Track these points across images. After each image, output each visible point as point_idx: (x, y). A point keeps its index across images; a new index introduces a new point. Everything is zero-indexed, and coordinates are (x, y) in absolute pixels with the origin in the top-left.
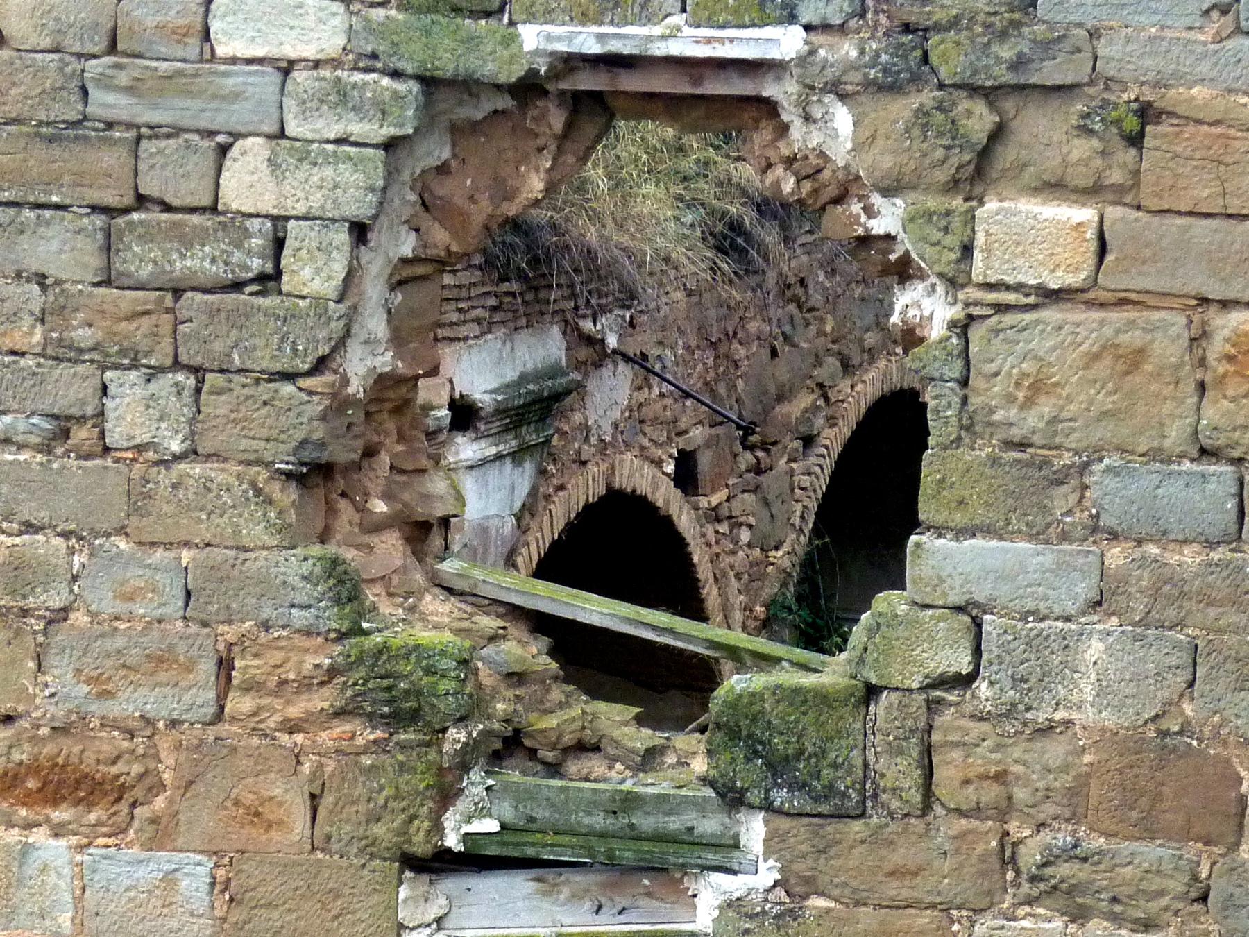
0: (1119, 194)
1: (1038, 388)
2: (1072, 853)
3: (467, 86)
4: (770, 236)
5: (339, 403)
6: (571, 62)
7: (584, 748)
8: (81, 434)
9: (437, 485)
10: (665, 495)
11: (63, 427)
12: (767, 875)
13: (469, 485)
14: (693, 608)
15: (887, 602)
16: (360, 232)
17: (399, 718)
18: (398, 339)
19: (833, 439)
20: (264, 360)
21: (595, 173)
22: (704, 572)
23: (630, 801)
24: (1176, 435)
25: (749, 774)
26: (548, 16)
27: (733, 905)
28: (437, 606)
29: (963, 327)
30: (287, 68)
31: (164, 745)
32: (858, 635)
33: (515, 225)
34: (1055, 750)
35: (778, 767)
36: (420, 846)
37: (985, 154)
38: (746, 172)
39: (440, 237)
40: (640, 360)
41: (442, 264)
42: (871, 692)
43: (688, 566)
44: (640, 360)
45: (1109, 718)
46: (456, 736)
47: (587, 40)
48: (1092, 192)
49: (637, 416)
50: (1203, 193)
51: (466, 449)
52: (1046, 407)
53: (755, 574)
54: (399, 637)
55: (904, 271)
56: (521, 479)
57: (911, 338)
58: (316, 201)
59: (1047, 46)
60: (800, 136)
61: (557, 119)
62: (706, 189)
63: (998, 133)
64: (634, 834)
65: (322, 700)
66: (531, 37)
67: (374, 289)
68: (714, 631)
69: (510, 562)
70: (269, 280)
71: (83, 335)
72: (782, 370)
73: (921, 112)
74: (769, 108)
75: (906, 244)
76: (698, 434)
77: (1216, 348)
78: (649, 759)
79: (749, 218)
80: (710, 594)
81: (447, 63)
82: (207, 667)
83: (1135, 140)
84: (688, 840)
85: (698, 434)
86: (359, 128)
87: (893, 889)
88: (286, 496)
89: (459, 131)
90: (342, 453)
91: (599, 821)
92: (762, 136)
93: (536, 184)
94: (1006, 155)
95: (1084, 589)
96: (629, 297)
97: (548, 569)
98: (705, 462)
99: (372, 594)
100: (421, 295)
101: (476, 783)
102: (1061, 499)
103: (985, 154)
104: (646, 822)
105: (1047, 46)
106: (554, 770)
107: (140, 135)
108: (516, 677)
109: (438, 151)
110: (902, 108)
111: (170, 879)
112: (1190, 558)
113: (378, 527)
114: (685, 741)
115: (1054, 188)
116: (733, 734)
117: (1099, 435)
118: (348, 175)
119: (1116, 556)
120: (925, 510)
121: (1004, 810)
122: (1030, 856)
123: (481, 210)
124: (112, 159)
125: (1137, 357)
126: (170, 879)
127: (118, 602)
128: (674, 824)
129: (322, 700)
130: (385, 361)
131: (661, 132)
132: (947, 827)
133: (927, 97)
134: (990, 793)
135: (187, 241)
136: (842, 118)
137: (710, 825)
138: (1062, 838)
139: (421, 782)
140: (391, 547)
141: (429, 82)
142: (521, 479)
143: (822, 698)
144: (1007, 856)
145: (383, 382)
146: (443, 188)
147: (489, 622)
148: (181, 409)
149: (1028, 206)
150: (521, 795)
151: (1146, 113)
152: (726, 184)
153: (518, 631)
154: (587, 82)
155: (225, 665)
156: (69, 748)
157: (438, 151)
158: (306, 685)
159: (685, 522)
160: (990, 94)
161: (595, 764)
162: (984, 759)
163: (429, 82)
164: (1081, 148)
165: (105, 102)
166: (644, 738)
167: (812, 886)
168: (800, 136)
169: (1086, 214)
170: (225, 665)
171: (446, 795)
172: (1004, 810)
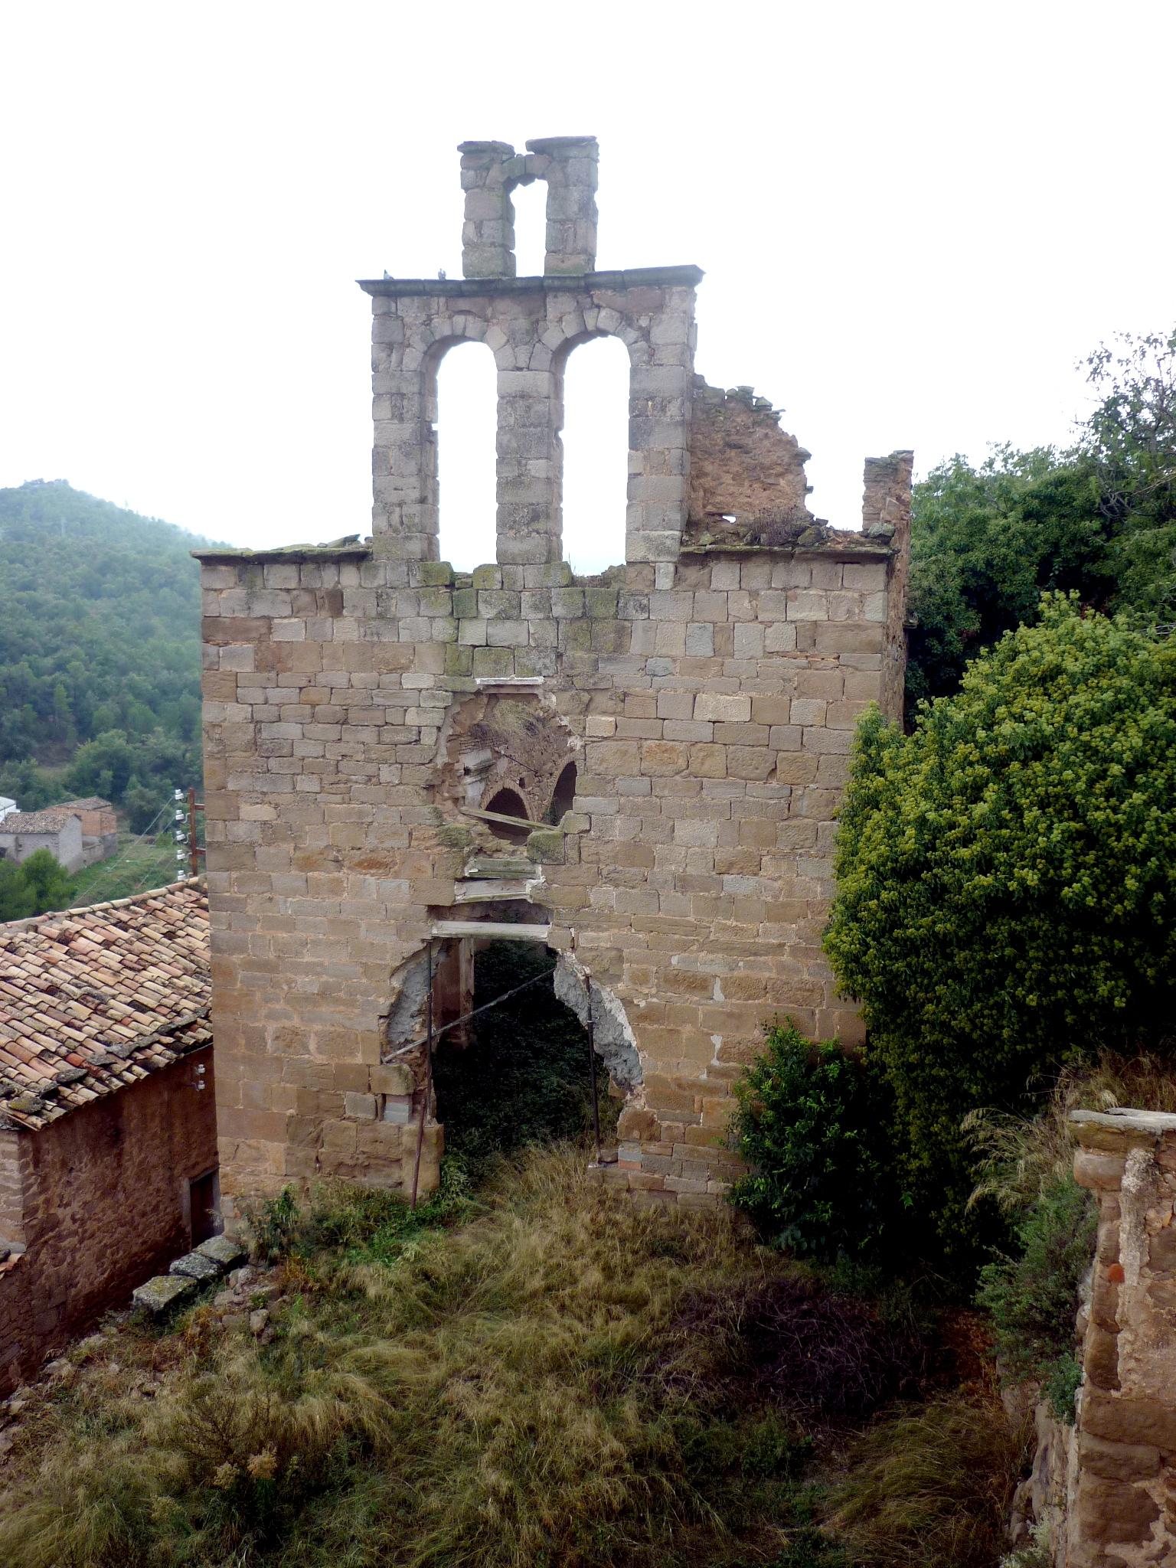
0: (620, 714)
1: (603, 761)
2: (615, 871)
3: (463, 693)
4: (540, 726)
5: (436, 770)
6: (488, 686)
7: (497, 851)
8: (374, 780)
9: (460, 789)
10: (517, 789)
11: (370, 778)
12: (542, 879)
13: (469, 788)
14: (525, 816)
15: (569, 813)
16: (439, 729)
17: (453, 845)
18: (449, 754)
19: (557, 773)
20: (418, 760)
21: (497, 712)
22: (527, 807)
23: (508, 863)
24: (635, 771)
25: (537, 856)
26: (482, 676)
27: (534, 887)
28: (461, 818)
29: (584, 747)
30: (420, 691)
31: (397, 853)
32: (562, 821)
33: (478, 725)
34: (610, 846)
35: (544, 853)
36: (459, 876)
37: (588, 705)
38: (532, 711)
39: (459, 729)
40: (510, 757)
41: (459, 736)
42: (566, 835)
43: (522, 805)
44: (510, 757)
45: (622, 839)
46: (467, 849)
47: (492, 681)
48: (613, 714)
49: (509, 770)
50: (639, 713)
51: (468, 779)
52: (605, 765)
53: (540, 806)
54: (453, 826)
55: (570, 734)
56: (482, 786)
57: (572, 750)
58: (428, 722)
59: (601, 679)
60: (544, 703)
61: (485, 700)
62: (524, 716)
63: (591, 700)
64: (510, 871)
65: (434, 842)
66: (478, 681)
67: (443, 742)
68: (531, 822)
69: (480, 806)
70: (417, 741)
71: (374, 756)
72: (544, 757)
73: (572, 696)
74: (536, 696)
75: (570, 728)
76: (524, 774)
77: (644, 749)
78: (513, 853)
79: (534, 722)
80: (529, 812)
81: (458, 687)
82: (406, 835)
83: (623, 701)
84: (522, 872)
85: (524, 774)
86: (438, 704)
87: (573, 882)
88: (424, 793)
89: (462, 704)
90: (436, 782)
91: (502, 868)
92: (535, 702)
93: (481, 716)
94: (592, 706)
95: (616, 808)
96: (506, 742)
97: (488, 809)
98: (526, 781)
99: (445, 816)
100: (455, 744)
101: (472, 860)
102: (609, 787)
103: (588, 705)
104: (513, 868)
105: (601, 679)
106: (490, 856)
107: (386, 708)
108: (481, 835)
109: (457, 709)
110: (568, 695)
111: (399, 886)
112: (640, 800)
113: (446, 800)
114: (522, 848)
115: (604, 713)
116: (533, 846)
117: (1088, 624)
118: (435, 715)
119: (622, 800)
120: (577, 791)
121: (598, 862)
122: (605, 873)
123: (468, 723)
124: (379, 714)
125: (625, 753)
126: (399, 886)
127: (345, 612)
128: (520, 868)
129: (434, 842)
130: (446, 760)
131: (511, 702)
132: (585, 866)
133: (574, 692)
134: (595, 858)
135: (397, 732)
136: (554, 698)
137: (528, 868)
138: (611, 868)
139: (458, 860)
140: (449, 804)
141: (454, 693)
142: (482, 786)
143: (554, 837)
144: (599, 873)
145: (446, 765)
146: (458, 718)
147: (474, 822)
148: (398, 773)
149: (598, 717)
150: (483, 863)
151: (625, 694)
152: (528, 714)
153: (481, 823)
154: (492, 691)
155: (410, 834)
156: (374, 855)
157: (457, 709)
158: (430, 838)
159: (522, 794)
160: (588, 691)
161: (500, 855)
162: (593, 850)
163: (454, 693)
164: (611, 703)
165: (378, 700)
166: (512, 848)
167: (553, 882)
168: (544, 703)
169: (612, 719)
170: (410, 834)
171: (465, 864)
172: (598, 862)
